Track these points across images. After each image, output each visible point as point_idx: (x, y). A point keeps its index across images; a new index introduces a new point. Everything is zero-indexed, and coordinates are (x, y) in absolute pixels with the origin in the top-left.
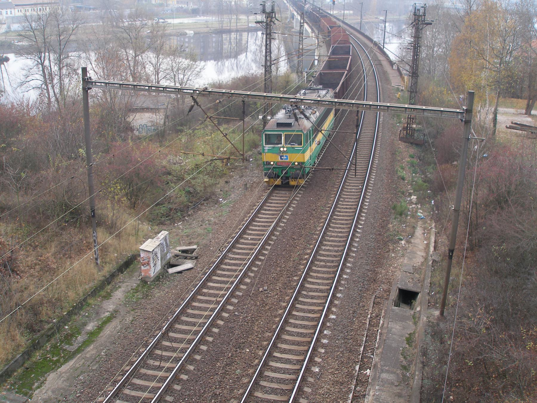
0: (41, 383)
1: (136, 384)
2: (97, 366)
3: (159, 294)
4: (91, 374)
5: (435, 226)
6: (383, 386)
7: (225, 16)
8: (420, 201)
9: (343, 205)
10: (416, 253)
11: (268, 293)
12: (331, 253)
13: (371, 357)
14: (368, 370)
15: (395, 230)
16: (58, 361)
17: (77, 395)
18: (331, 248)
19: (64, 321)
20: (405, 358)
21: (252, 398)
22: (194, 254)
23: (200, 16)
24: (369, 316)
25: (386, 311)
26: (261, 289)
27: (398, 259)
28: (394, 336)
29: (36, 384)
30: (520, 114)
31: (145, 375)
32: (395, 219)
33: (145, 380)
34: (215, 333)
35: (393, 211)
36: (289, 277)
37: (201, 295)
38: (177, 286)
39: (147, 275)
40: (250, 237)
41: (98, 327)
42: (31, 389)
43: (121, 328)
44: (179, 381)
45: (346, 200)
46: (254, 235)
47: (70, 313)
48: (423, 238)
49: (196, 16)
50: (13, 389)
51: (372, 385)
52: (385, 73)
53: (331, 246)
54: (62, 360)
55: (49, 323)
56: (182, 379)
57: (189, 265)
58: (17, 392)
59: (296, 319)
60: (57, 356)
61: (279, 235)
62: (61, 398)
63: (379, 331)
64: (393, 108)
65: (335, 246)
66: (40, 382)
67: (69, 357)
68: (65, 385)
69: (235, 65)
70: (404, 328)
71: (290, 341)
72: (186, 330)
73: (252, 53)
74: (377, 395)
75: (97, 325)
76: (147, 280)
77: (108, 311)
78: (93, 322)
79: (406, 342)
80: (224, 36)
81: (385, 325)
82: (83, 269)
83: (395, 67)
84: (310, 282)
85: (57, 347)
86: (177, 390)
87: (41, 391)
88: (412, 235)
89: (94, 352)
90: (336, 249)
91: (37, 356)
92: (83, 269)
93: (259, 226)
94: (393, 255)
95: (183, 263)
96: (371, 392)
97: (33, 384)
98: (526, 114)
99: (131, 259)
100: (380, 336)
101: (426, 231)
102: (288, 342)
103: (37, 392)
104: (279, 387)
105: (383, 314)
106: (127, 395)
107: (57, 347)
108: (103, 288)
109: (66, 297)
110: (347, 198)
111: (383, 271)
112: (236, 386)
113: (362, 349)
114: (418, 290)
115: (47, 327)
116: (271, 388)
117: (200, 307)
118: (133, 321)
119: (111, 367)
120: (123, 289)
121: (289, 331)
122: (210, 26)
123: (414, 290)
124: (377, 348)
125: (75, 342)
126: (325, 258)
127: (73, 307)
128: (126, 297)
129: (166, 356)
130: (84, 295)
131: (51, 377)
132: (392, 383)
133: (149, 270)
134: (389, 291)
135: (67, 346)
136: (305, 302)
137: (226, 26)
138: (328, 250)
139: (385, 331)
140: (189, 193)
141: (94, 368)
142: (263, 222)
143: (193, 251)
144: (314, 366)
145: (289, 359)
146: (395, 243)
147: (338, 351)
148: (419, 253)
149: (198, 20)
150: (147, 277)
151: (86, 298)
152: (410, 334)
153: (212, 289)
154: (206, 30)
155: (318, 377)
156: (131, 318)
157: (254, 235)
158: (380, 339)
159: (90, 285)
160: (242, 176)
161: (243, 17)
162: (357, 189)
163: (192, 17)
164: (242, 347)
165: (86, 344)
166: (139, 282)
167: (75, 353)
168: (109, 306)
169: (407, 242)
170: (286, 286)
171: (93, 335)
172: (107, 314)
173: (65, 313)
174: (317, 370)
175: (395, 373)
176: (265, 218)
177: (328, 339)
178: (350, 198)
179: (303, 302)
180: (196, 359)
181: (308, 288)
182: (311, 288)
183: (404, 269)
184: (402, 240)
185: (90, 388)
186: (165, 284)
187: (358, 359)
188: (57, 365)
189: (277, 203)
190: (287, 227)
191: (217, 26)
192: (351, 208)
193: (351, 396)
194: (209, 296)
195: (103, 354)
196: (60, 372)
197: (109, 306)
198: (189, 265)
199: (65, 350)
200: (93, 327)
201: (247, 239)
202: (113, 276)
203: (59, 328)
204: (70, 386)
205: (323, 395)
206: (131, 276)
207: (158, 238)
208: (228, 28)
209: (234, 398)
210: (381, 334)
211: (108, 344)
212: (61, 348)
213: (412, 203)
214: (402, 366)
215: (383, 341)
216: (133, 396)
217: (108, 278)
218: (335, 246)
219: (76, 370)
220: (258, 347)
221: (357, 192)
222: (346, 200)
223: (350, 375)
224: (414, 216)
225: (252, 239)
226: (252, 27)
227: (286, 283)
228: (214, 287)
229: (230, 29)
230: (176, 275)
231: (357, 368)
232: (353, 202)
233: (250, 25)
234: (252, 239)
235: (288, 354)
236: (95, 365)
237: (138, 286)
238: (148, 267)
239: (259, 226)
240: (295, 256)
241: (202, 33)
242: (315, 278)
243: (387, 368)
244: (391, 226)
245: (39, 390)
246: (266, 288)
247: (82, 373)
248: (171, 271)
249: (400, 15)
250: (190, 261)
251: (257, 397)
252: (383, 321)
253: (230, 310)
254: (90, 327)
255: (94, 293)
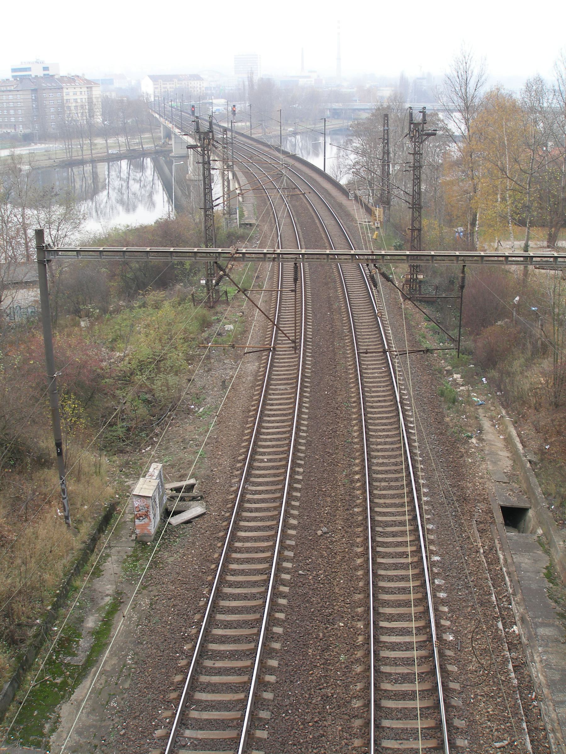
0: (55, 723)
1: (201, 701)
2: (129, 682)
3: (172, 559)
4: (126, 695)
5: (507, 413)
6: (547, 646)
7: (74, 142)
8: (469, 379)
9: (372, 397)
10: (497, 454)
11: (331, 536)
12: (388, 468)
13: (509, 608)
14: (515, 627)
15: (456, 426)
16: (65, 683)
17: (122, 733)
18: (385, 461)
19: (51, 619)
20: (556, 602)
21: (380, 693)
22: (195, 492)
23: (36, 144)
24: (482, 551)
25: (500, 540)
26: (319, 533)
27: (479, 466)
28: (528, 574)
29: (47, 726)
30: (541, 247)
31: (209, 684)
32: (449, 409)
33: (213, 692)
34: (284, 605)
35: (443, 399)
36: (348, 509)
37: (235, 552)
38: (194, 543)
39: (146, 532)
40: (265, 458)
41: (103, 621)
42: (42, 735)
43: (140, 618)
44: (265, 686)
45: (373, 389)
46: (269, 453)
47: (56, 606)
48: (495, 432)
49: (29, 145)
50: (14, 740)
51: (532, 647)
52: (340, 206)
53: (383, 457)
54: (70, 681)
55: (31, 627)
56: (268, 682)
57: (196, 510)
58: (22, 744)
59: (386, 569)
60: (60, 676)
61: (306, 450)
62: (96, 742)
63: (504, 569)
64: (438, 258)
65: (390, 457)
66: (52, 721)
67: (79, 675)
68: (94, 720)
69: (94, 210)
70: (535, 561)
71: (393, 601)
72: (239, 607)
73: (116, 191)
74: (546, 660)
75: (101, 618)
76: (145, 539)
77: (107, 595)
78: (92, 615)
79: (546, 580)
80: (75, 170)
81: (509, 561)
82: (51, 535)
83: (351, 197)
84: (380, 513)
85: (54, 662)
86: (269, 700)
87: (60, 736)
88: (481, 429)
89: (114, 661)
90: (392, 460)
91: (31, 682)
92: (51, 535)
93: (270, 440)
94: (470, 461)
95: (188, 508)
96: (535, 657)
97: (43, 726)
98: (548, 247)
99: (109, 510)
100: (509, 577)
101: (496, 421)
102: (391, 603)
103: (53, 738)
104: (410, 671)
105: (498, 546)
106: (196, 719)
107: (54, 662)
108: (85, 560)
109: (43, 581)
110: (374, 387)
111: (469, 485)
112: (350, 680)
113: (494, 598)
114: (527, 505)
115: (31, 633)
116: (399, 674)
117: (243, 570)
118: (151, 604)
119: (153, 681)
120: (114, 558)
121: (385, 587)
122: (53, 157)
123: (522, 505)
124: (514, 594)
125: (78, 650)
126: (384, 476)
127: (57, 595)
128: (125, 570)
129: (227, 651)
130: (65, 575)
131: (65, 709)
132: (557, 640)
133: (148, 524)
134: (491, 512)
135: (69, 658)
136: (387, 543)
137: (76, 155)
138: (383, 463)
139: (512, 569)
140: (147, 402)
141: (127, 686)
142: (273, 434)
143: (190, 488)
144: (445, 633)
145: (404, 628)
146: (464, 444)
147: (467, 607)
148: (500, 453)
149: (34, 149)
150: (145, 535)
151: (70, 579)
152: (547, 568)
153: (248, 541)
154: (48, 163)
155: (456, 646)
156: (147, 601)
157: (269, 453)
158: (511, 581)
159: (68, 558)
160: (210, 370)
161: (99, 141)
162: (381, 373)
163: (24, 146)
164: (331, 621)
165: (97, 649)
166: (134, 545)
167: (86, 667)
168: (106, 587)
169: (479, 439)
170: (349, 522)
171: (101, 635)
172: (108, 600)
173: (49, 608)
174: (451, 638)
175: (553, 625)
176: (273, 428)
177: (445, 591)
178: (377, 387)
179: (383, 542)
180: (274, 649)
181: (381, 522)
182: (386, 522)
183: (494, 477)
184: (471, 437)
185: (135, 718)
186: (175, 541)
187: (496, 613)
188: (65, 691)
189: (281, 404)
190: (311, 438)
191: (62, 156)
192: (385, 401)
193: (510, 667)
194: (247, 552)
195: (130, 662)
196: (76, 700)
197: (106, 587)
198: (196, 510)
199: (68, 665)
200: (95, 622)
201: (262, 461)
202: (94, 540)
203: (45, 633)
204: (102, 720)
205: (476, 671)
206: (117, 536)
207: (152, 476)
208: (80, 158)
209: (355, 697)
210: (509, 573)
211: (131, 646)
212: (61, 663)
213: (457, 384)
214: (558, 614)
215: (517, 584)
216: (207, 720)
217: (89, 545)
218: (390, 457)
219: (100, 693)
220: (353, 617)
221: (382, 377)
222: (373, 389)
223: (496, 638)
224: (470, 403)
225: (270, 461)
226: (113, 154)
227: (348, 519)
228: (248, 537)
229: (82, 159)
230: (185, 526)
231: (500, 625)
232: (383, 391)
233: (110, 151)
234: (270, 461)
235: (399, 621)
236: (125, 680)
237: (135, 550)
238: (146, 520)
239: (270, 440)
240: (341, 477)
241: (43, 167)
242: (383, 507)
243: (540, 620)
244: (448, 419)
245: (55, 734)
246: (325, 529)
247: (111, 696)
248: (175, 520)
249: (315, 124)
250: (195, 503)
251: (386, 691)
252: (504, 555)
253: (288, 569)
254: (91, 623)
255: (79, 567)
